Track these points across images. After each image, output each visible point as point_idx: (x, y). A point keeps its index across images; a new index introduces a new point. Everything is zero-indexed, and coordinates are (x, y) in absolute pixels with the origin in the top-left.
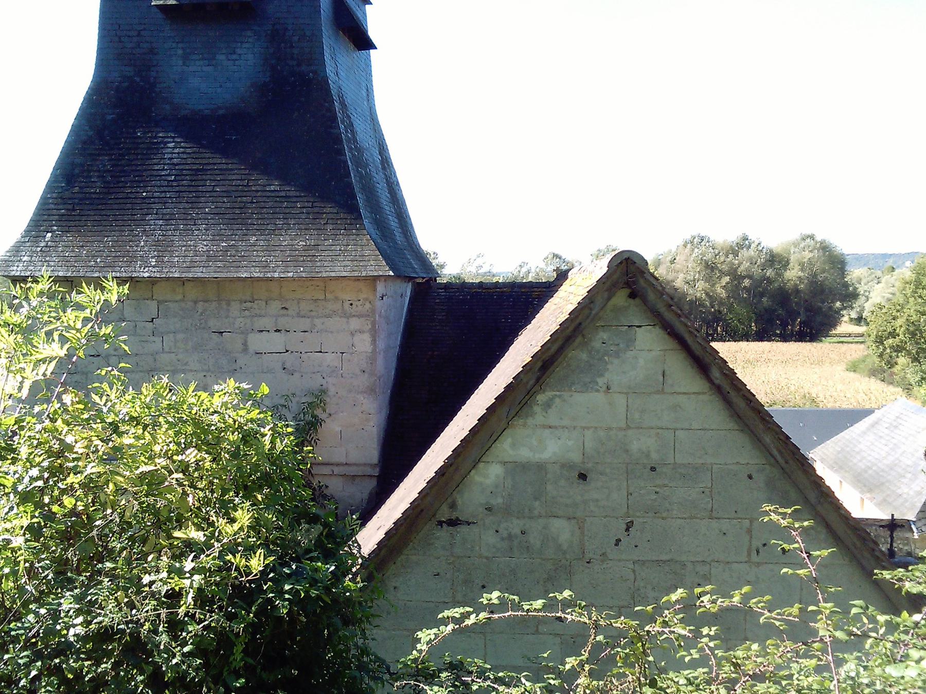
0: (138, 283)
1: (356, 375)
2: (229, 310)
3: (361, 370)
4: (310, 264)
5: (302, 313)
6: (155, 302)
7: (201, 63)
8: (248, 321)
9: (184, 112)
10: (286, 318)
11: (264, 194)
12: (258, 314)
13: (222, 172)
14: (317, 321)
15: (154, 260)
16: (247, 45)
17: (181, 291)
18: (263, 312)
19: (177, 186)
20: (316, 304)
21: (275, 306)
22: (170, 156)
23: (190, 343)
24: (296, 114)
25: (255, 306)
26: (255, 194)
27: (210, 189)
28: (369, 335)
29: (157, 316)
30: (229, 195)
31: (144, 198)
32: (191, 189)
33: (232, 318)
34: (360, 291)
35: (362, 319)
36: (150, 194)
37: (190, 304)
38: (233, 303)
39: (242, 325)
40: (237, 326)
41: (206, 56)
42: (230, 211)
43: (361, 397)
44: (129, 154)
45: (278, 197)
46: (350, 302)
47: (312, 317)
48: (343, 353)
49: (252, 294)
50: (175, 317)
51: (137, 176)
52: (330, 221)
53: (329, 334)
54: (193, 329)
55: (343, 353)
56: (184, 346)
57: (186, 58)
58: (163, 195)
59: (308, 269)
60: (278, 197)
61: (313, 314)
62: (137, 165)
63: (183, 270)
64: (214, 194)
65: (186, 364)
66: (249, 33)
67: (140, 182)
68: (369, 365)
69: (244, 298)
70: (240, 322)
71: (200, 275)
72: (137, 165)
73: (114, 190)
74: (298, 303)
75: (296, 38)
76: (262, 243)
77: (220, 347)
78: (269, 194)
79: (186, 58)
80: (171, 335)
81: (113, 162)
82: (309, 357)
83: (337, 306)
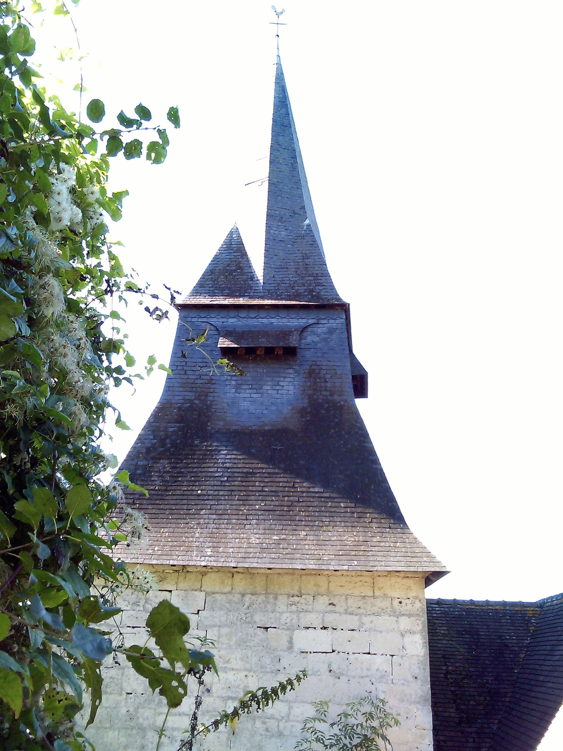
0: (189, 574)
1: (408, 682)
2: (275, 604)
3: (413, 676)
4: (363, 558)
5: (350, 610)
6: (203, 594)
7: (251, 391)
8: (295, 616)
9: (234, 428)
10: (334, 615)
11: (309, 495)
12: (305, 609)
13: (270, 476)
14: (366, 620)
15: (209, 550)
16: (288, 379)
17: (230, 583)
18: (310, 608)
19: (229, 486)
20: (365, 601)
21: (323, 601)
22: (223, 461)
23: (234, 639)
24: (332, 431)
25: (303, 601)
26: (300, 494)
27: (260, 489)
28: (420, 637)
29: (203, 609)
30: (277, 494)
31: (199, 495)
32: (243, 488)
33: (279, 612)
34: (409, 588)
35: (413, 619)
36: (204, 492)
37: (237, 597)
38: (280, 597)
39: (288, 620)
40: (283, 621)
41: (254, 386)
42: (279, 508)
43: (414, 708)
44: (186, 459)
45: (322, 497)
46: (399, 600)
47: (361, 615)
48: (393, 656)
49: (300, 588)
50: (221, 609)
51: (193, 477)
52: (374, 520)
53: (378, 633)
54: (239, 623)
55: (393, 656)
56: (227, 642)
57: (238, 387)
58: (216, 493)
59: (362, 563)
60: (322, 497)
61: (362, 611)
62: (193, 468)
63: (237, 560)
64: (264, 493)
65: (228, 661)
66: (291, 371)
67: (195, 481)
68: (422, 671)
69: (292, 592)
70: (285, 618)
71: (255, 565)
72: (193, 468)
73: (173, 488)
74: (346, 599)
75: (329, 376)
76: (312, 538)
77: (265, 644)
78: (313, 495)
79: (238, 387)
80: (216, 629)
81: (172, 465)
82: (356, 659)
83: (386, 604)
